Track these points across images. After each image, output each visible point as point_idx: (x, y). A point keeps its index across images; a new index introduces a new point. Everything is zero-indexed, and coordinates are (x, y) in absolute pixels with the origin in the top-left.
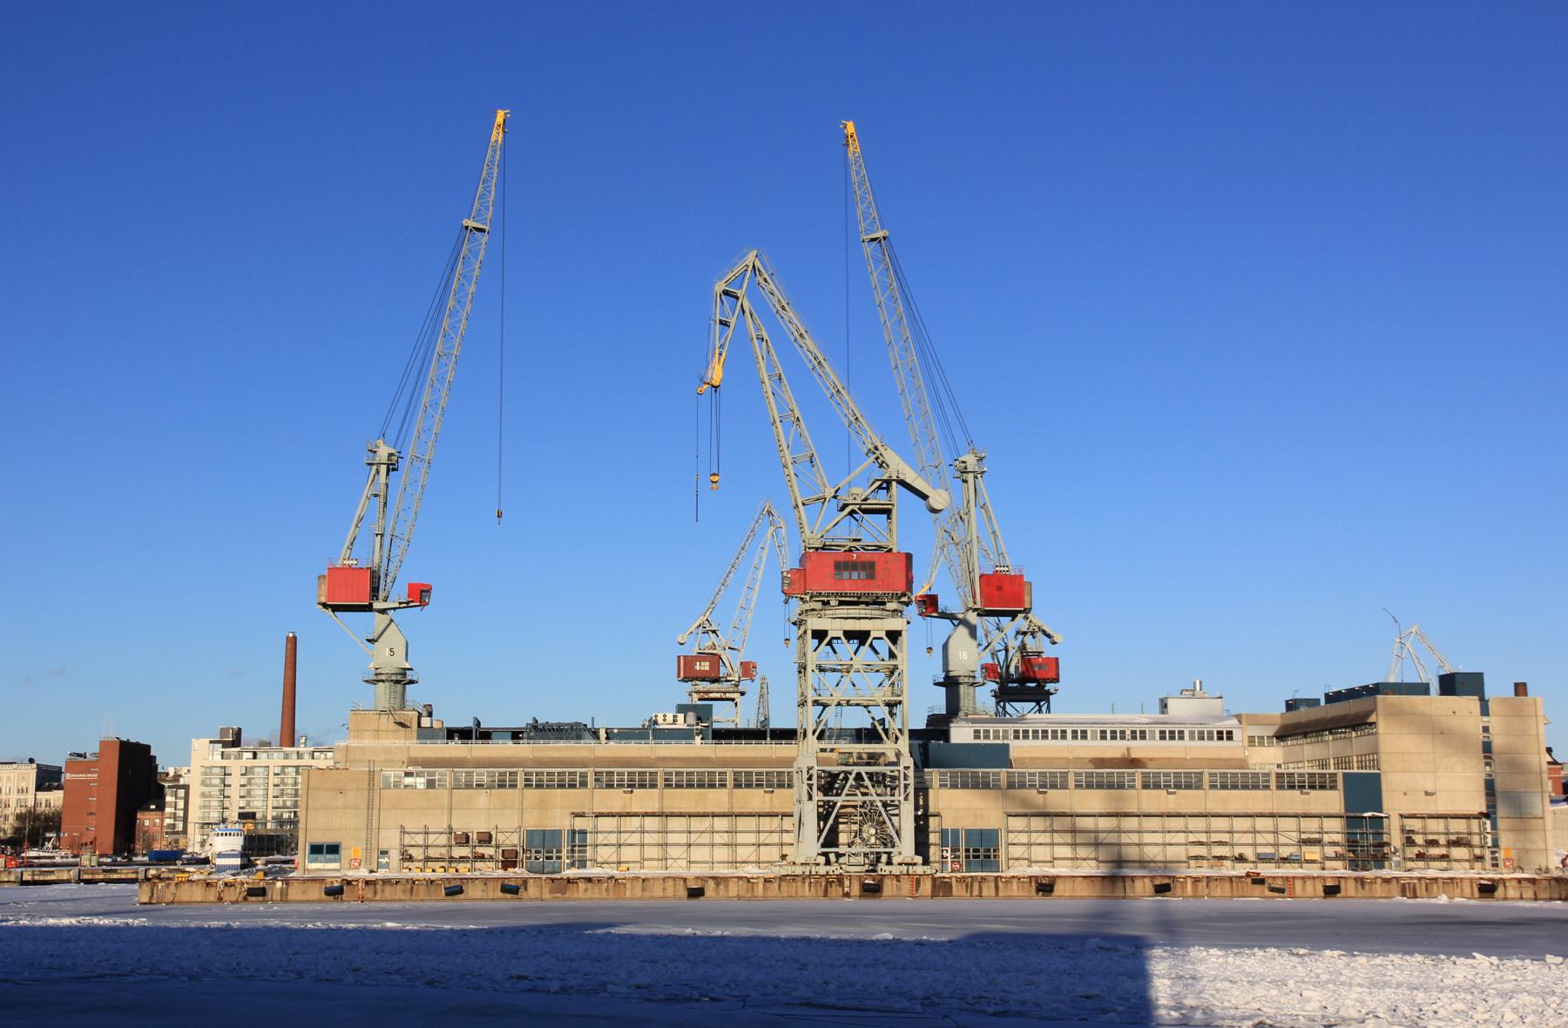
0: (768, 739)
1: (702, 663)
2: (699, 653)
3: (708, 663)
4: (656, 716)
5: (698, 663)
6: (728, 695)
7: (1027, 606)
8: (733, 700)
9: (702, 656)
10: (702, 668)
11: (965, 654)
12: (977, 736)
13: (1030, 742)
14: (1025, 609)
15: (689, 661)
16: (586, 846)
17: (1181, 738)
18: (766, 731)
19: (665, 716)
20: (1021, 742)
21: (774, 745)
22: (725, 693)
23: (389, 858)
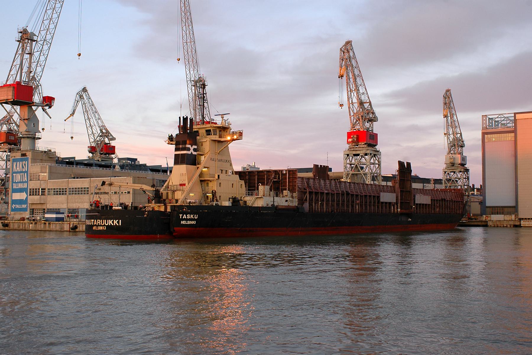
10: (11, 139)
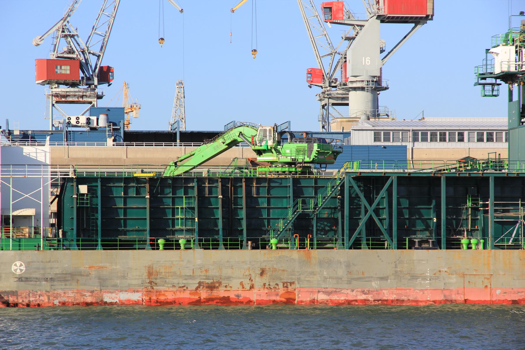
0: (178, 141)
1: (63, 67)
2: (58, 57)
3: (68, 67)
4: (69, 119)
5: (59, 67)
6: (85, 99)
7: (429, 12)
8: (91, 103)
9: (62, 60)
10: (63, 72)
11: (368, 59)
12: (377, 138)
13: (428, 145)
14: (428, 16)
15: (51, 65)
16: (384, 241)
17: (461, 140)
18: (176, 134)
19: (78, 118)
20: (419, 145)
21: (183, 147)
22: (82, 97)
23: (161, 250)
